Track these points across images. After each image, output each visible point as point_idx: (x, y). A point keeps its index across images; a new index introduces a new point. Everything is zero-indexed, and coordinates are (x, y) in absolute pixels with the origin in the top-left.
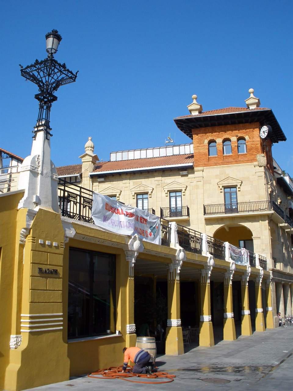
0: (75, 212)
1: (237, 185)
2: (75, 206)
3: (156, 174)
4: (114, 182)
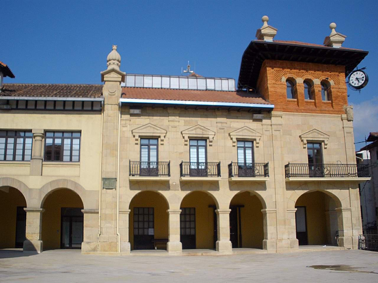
1: (160, 137)
3: (218, 113)
4: (155, 118)
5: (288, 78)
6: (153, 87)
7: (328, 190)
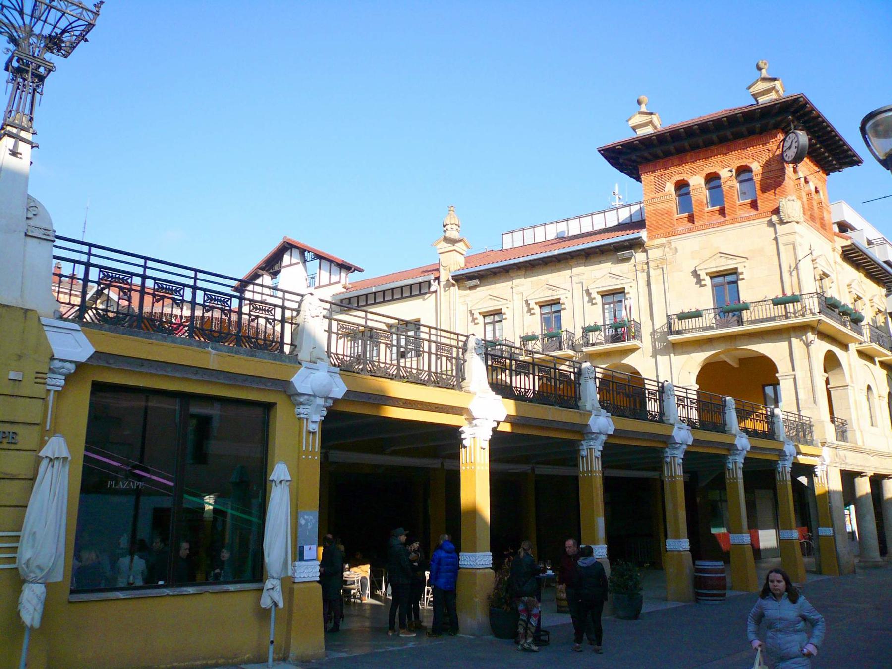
0: (527, 387)
2: (527, 379)
7: (749, 347)
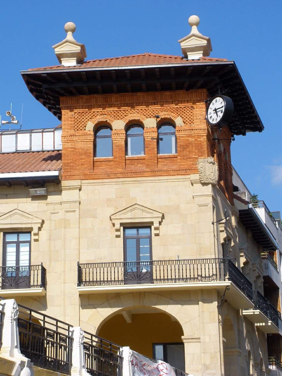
5: (129, 122)
6: (44, 149)
7: (157, 307)
